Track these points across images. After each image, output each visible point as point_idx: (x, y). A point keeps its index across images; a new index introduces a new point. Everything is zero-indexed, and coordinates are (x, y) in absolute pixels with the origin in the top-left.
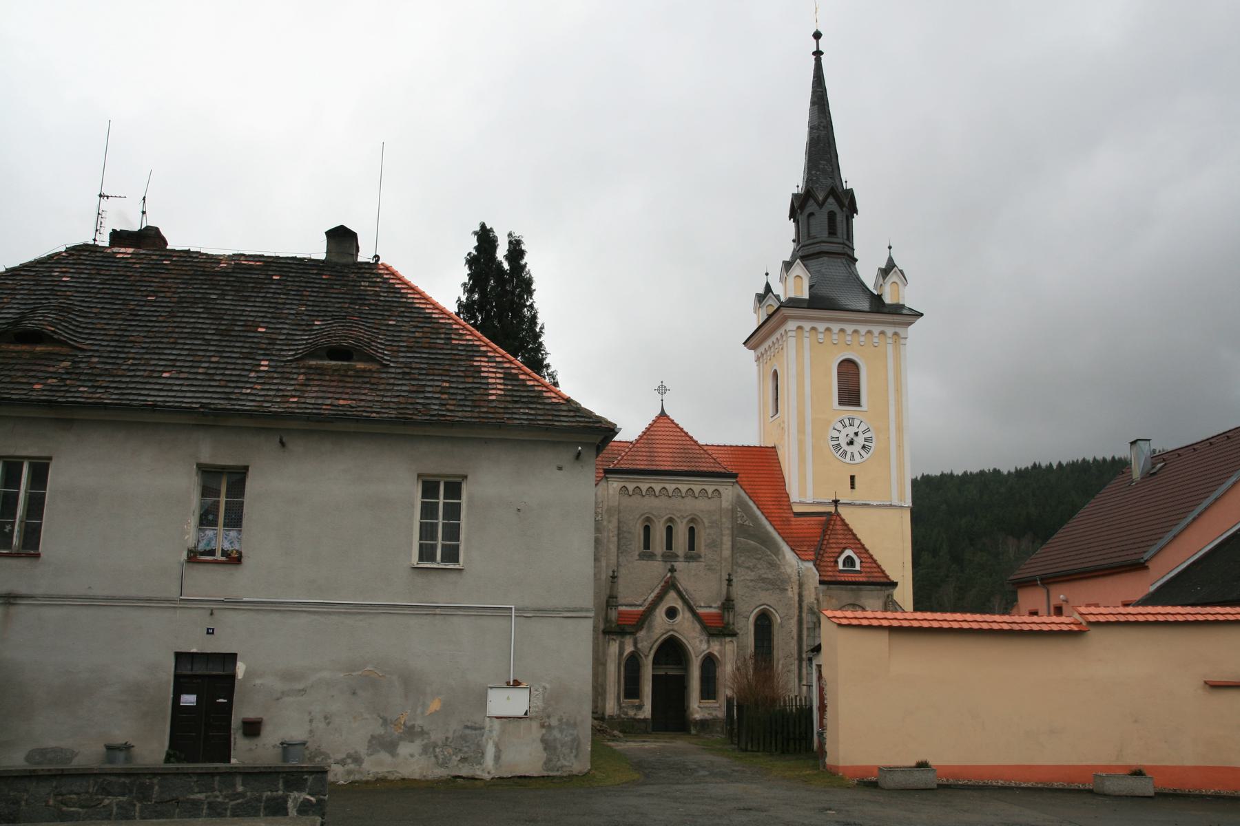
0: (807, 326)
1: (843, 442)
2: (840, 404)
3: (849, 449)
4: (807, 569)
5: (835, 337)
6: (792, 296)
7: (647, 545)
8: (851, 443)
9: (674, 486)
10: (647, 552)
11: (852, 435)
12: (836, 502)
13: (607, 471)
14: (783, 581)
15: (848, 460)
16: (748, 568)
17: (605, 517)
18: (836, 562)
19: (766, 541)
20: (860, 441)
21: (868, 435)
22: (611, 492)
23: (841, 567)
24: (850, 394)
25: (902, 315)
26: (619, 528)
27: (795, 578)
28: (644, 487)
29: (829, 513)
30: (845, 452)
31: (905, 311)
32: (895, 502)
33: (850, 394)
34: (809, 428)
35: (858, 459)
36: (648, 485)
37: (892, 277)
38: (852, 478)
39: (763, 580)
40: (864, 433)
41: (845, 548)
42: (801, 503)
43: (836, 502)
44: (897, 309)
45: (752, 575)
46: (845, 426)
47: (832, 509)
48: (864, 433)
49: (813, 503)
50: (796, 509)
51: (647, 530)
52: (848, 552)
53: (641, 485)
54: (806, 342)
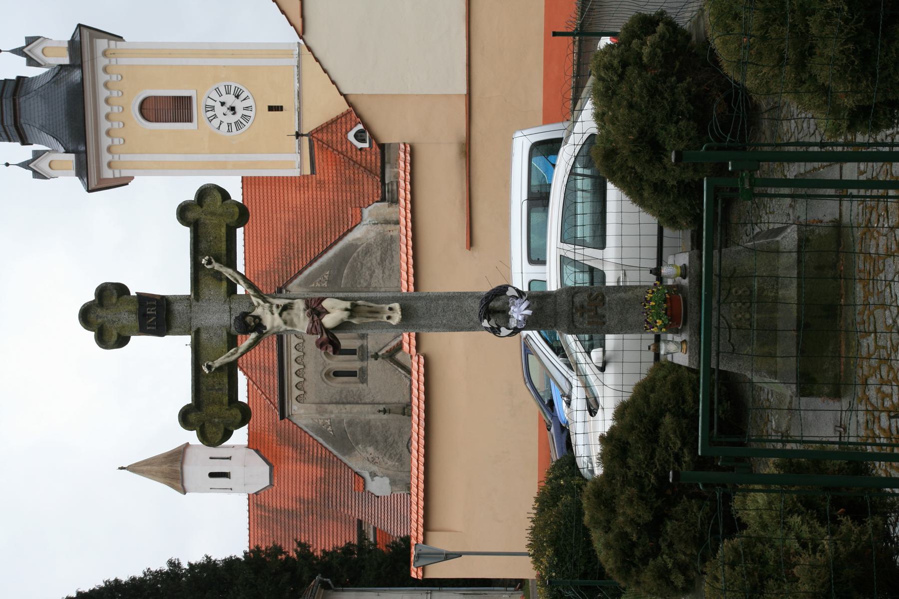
0: (106, 157)
1: (232, 119)
2: (190, 120)
3: (240, 111)
4: (370, 215)
5: (114, 78)
6: (74, 172)
7: (352, 374)
8: (233, 109)
9: (294, 351)
10: (359, 375)
11: (225, 109)
12: (298, 135)
13: (282, 417)
14: (383, 240)
15: (252, 114)
16: (371, 276)
17: (327, 416)
18: (361, 149)
19: (344, 258)
20: (230, 100)
21: (223, 91)
22: (302, 411)
23: (366, 145)
24: (179, 109)
25: (82, 41)
26: (337, 403)
27: (380, 228)
28: (295, 380)
29: (310, 140)
30: (243, 116)
31: (78, 39)
32: (294, 62)
33: (179, 109)
34: (221, 157)
35: (250, 102)
36: (294, 376)
37: (36, 51)
38: (271, 109)
39: (382, 261)
40: (221, 95)
41: (347, 139)
42: (301, 167)
43: (298, 135)
44: (75, 47)
45: (378, 272)
46: (215, 116)
47: (306, 140)
48: (221, 95)
49: (301, 153)
50: (307, 171)
51: (337, 374)
52: (351, 136)
53: (294, 383)
54: (125, 158)
